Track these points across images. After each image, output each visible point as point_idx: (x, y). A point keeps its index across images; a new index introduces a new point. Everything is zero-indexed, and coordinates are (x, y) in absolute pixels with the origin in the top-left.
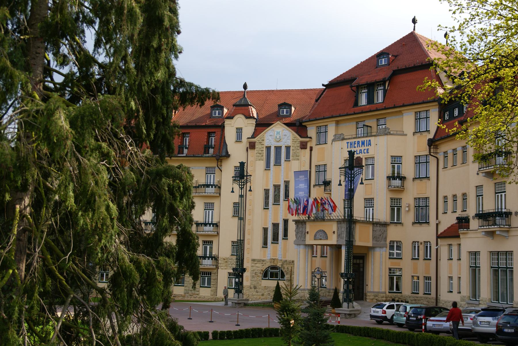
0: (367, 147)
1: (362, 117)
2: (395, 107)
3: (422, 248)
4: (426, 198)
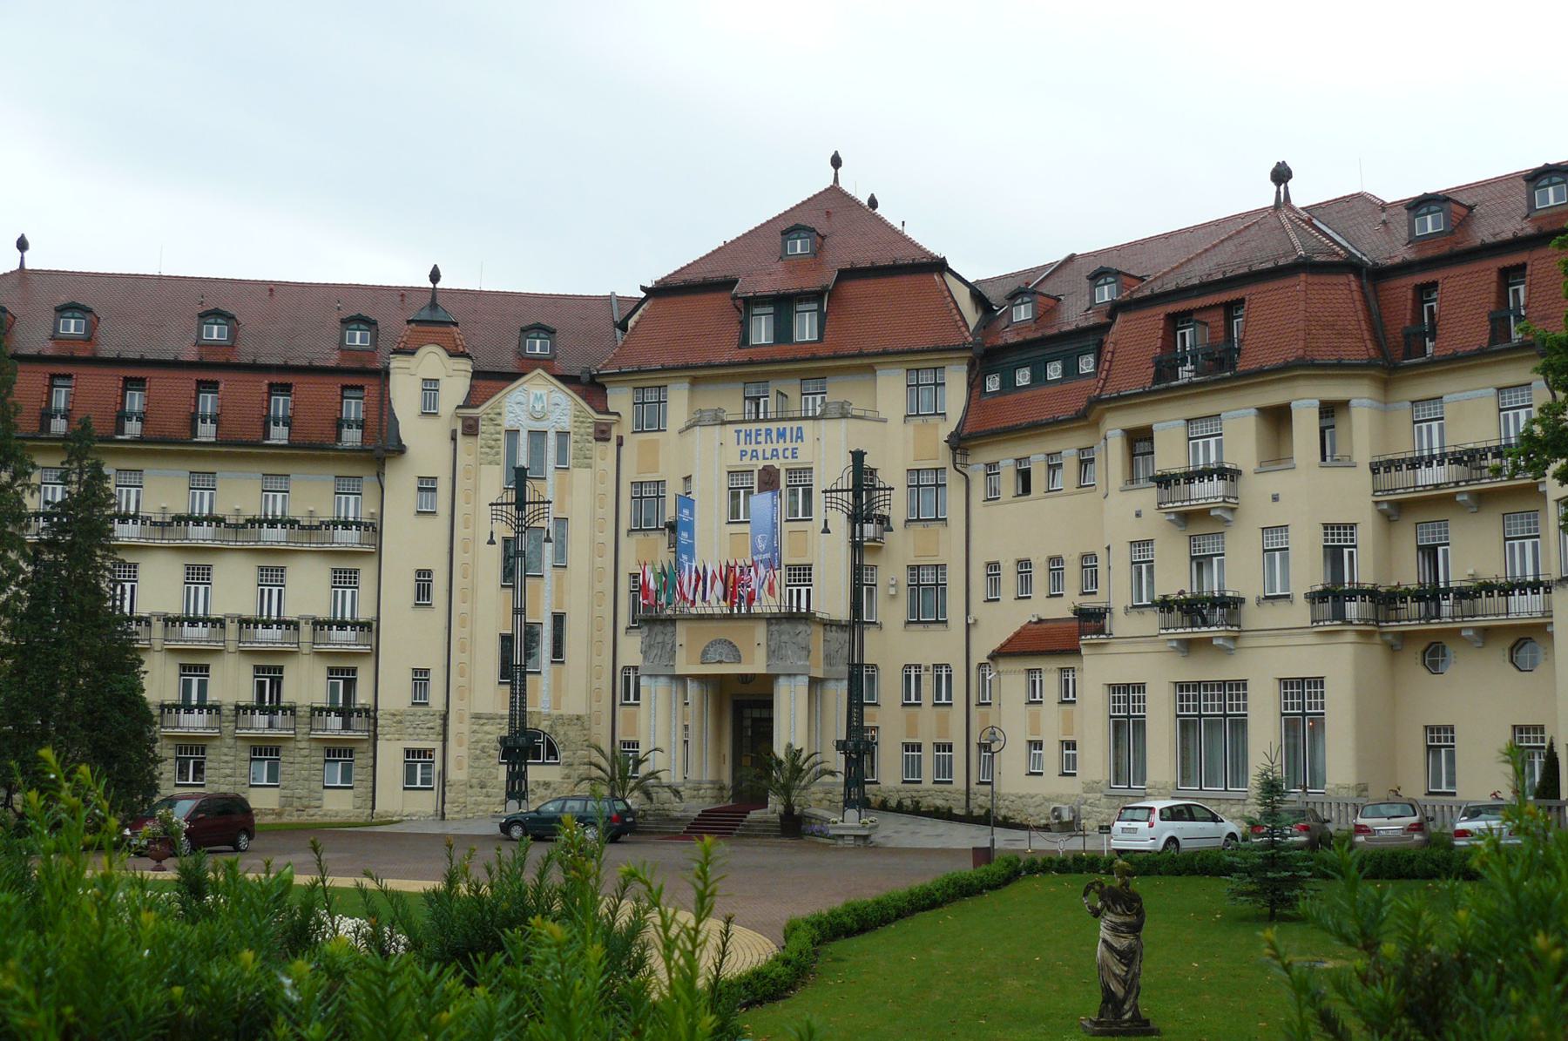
0: (794, 445)
2: (861, 355)
4: (939, 568)
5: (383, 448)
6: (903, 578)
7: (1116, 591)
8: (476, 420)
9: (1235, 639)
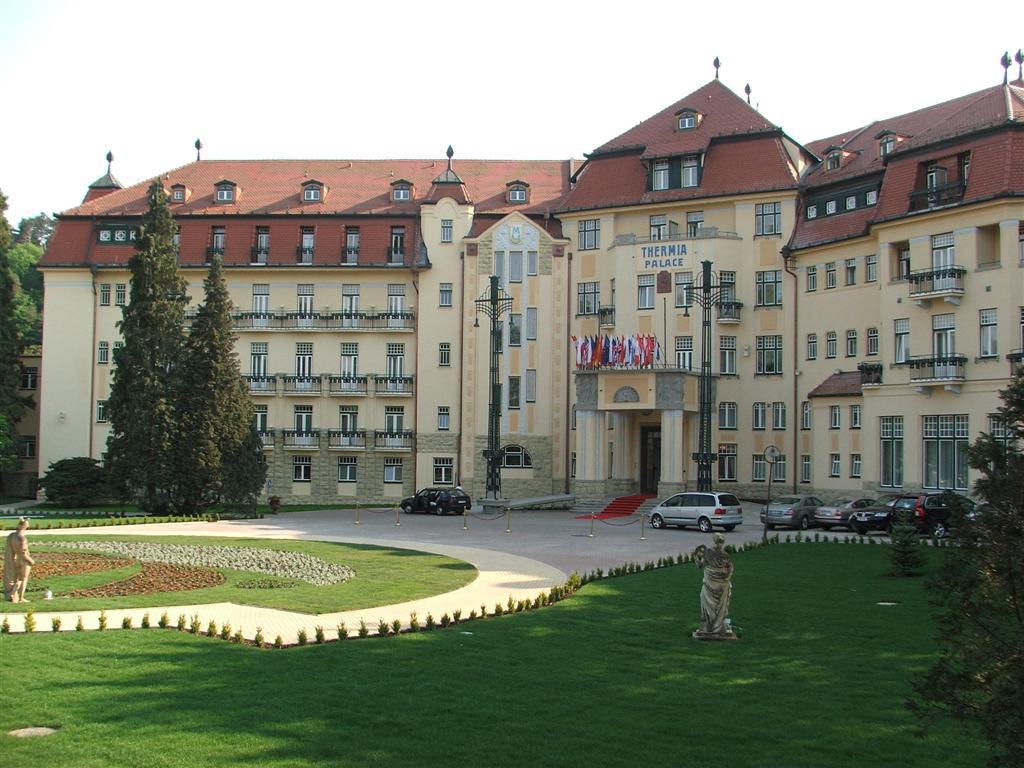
1: (662, 209)
3: (769, 411)
5: (417, 265)
6: (753, 343)
7: (886, 356)
8: (476, 245)
9: (960, 386)
